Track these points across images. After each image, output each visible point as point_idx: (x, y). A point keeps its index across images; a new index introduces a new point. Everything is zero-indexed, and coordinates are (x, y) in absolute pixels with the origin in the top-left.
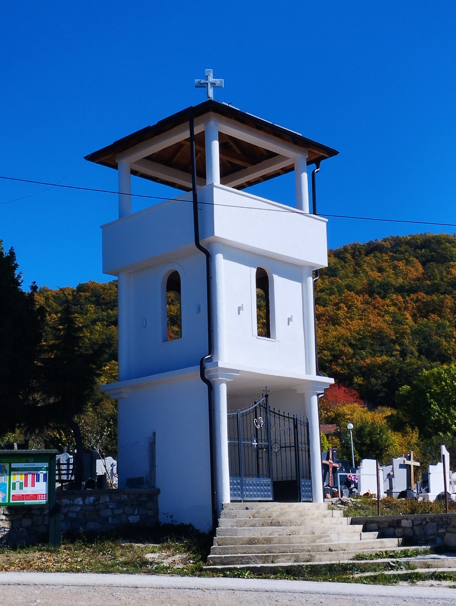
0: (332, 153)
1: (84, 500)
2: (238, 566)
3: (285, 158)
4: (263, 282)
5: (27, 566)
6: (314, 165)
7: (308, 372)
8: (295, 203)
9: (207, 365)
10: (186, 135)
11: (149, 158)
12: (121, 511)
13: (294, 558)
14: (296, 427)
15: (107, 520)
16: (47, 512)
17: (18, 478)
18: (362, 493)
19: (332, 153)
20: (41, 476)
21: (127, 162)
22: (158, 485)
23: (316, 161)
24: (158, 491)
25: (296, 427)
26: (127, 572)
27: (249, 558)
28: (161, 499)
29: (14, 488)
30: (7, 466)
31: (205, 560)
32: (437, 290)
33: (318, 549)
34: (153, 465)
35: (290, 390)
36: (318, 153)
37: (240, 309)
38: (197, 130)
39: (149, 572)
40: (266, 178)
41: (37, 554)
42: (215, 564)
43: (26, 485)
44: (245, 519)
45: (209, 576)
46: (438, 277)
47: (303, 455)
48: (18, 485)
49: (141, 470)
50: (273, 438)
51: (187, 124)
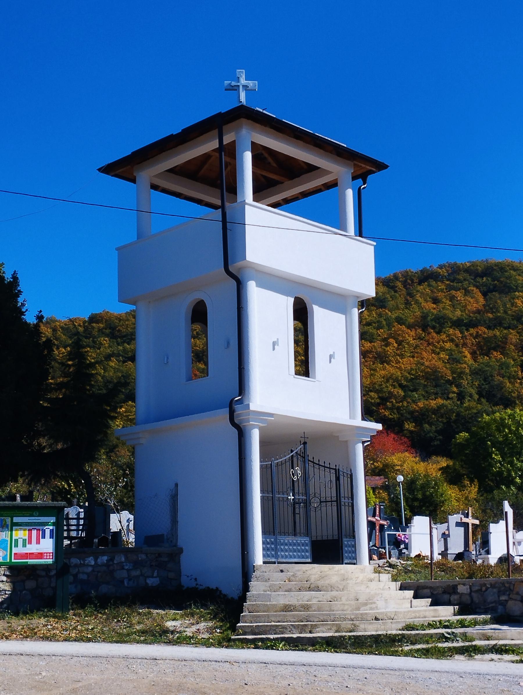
0: (381, 166)
1: (96, 560)
2: (272, 637)
3: (327, 172)
4: (301, 313)
5: (30, 634)
6: (360, 181)
7: (352, 416)
8: (339, 223)
9: (236, 407)
10: (214, 144)
11: (172, 171)
12: (138, 573)
13: (334, 628)
14: (338, 479)
15: (123, 582)
16: (53, 573)
17: (20, 534)
18: (413, 555)
19: (381, 166)
20: (48, 533)
21: (147, 174)
22: (181, 543)
23: (364, 177)
24: (181, 551)
25: (338, 479)
26: (145, 642)
27: (284, 627)
28: (184, 559)
29: (16, 546)
30: (8, 520)
31: (233, 629)
32: (500, 324)
33: (363, 618)
34: (174, 521)
35: (331, 437)
36: (365, 167)
37: (274, 344)
38: (227, 139)
39: (170, 642)
40: (305, 195)
41: (43, 621)
42: (245, 634)
43: (30, 542)
44: (281, 583)
45: (238, 647)
46: (501, 309)
47: (345, 511)
48: (20, 542)
49: (162, 526)
50: (312, 491)
51: (216, 132)
